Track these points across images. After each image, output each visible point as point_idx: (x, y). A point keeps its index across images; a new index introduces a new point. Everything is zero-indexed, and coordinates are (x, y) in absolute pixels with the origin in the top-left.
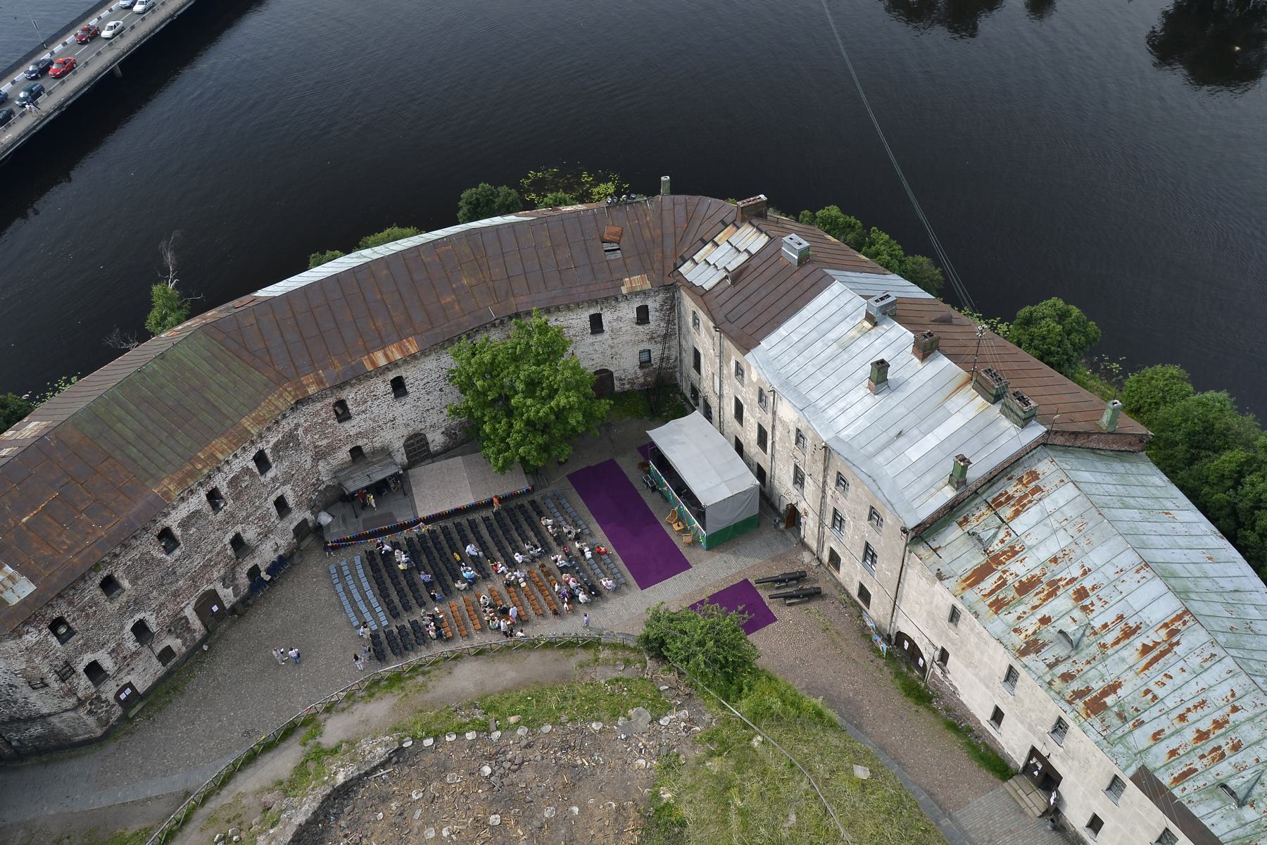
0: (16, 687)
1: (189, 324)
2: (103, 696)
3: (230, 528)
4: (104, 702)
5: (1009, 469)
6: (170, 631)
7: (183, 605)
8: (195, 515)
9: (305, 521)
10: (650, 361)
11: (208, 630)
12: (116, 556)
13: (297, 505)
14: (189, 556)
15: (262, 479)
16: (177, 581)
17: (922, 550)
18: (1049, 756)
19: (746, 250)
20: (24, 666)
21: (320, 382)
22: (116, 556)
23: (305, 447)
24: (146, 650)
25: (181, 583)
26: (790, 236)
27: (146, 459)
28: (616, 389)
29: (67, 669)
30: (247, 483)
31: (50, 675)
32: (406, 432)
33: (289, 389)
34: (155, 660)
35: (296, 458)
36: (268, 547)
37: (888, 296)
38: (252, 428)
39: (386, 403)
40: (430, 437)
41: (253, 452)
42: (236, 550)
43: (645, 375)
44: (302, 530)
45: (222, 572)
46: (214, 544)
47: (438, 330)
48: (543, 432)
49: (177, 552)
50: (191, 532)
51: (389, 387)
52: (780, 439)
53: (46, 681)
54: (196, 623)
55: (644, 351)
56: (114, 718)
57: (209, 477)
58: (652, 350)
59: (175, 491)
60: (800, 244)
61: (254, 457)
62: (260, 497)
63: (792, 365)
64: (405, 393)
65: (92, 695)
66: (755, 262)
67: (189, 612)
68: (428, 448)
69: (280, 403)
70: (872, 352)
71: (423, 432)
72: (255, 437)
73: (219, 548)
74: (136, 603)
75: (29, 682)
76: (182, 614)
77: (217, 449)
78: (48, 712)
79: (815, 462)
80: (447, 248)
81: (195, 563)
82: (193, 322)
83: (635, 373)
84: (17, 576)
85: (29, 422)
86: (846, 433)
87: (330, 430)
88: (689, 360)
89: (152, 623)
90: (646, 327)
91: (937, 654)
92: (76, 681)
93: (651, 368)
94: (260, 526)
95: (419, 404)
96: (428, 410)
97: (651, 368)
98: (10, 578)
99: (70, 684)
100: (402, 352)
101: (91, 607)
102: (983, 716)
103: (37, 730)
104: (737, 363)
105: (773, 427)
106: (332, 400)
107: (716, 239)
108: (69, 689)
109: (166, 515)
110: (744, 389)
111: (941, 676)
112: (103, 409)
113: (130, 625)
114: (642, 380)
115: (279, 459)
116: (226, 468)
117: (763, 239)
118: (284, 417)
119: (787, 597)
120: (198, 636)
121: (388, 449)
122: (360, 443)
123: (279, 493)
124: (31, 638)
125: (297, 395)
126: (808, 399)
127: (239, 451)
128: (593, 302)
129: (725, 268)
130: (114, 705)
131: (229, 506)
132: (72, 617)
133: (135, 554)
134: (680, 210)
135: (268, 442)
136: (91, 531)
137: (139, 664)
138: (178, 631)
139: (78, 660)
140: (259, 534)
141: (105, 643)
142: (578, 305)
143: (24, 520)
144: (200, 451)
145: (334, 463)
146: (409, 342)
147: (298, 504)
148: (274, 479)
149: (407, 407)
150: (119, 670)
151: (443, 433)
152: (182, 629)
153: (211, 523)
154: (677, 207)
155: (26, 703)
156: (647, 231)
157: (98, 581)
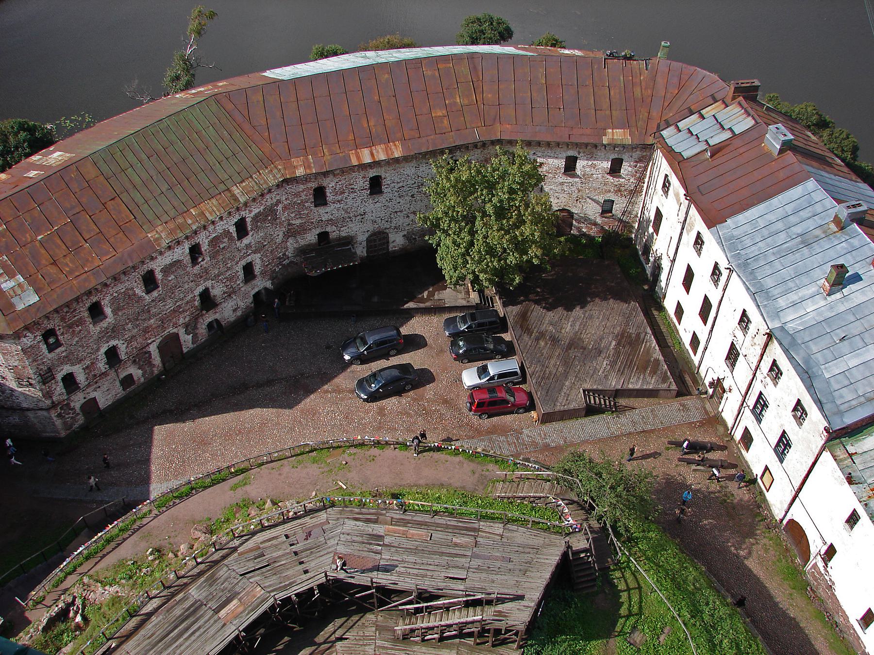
1: (202, 89)
2: (72, 405)
3: (202, 282)
8: (177, 264)
11: (164, 367)
13: (261, 273)
14: (164, 300)
15: (238, 243)
16: (150, 319)
19: (730, 129)
21: (307, 166)
23: (280, 223)
24: (112, 373)
26: (776, 126)
29: (49, 374)
30: (224, 245)
32: (371, 227)
34: (118, 383)
36: (230, 305)
40: (392, 237)
45: (187, 319)
46: (186, 293)
47: (424, 140)
49: (155, 294)
50: (170, 279)
54: (157, 359)
57: (195, 232)
60: (785, 135)
61: (236, 222)
63: (753, 248)
64: (380, 192)
67: (153, 349)
68: (388, 246)
70: (832, 254)
72: (241, 205)
73: (189, 297)
74: (113, 331)
78: (27, 406)
81: (167, 307)
82: (206, 88)
84: (26, 285)
87: (306, 212)
89: (123, 351)
91: (825, 548)
96: (396, 212)
99: (49, 387)
100: (387, 154)
103: (15, 419)
107: (703, 112)
109: (152, 259)
111: (822, 570)
113: (104, 349)
115: (256, 228)
116: (211, 228)
117: (749, 122)
122: (329, 229)
126: (762, 285)
129: (706, 141)
130: (78, 414)
131: (205, 261)
135: (250, 211)
137: (105, 384)
138: (141, 363)
139: (59, 369)
140: (224, 293)
141: (82, 360)
143: (39, 238)
145: (302, 243)
146: (395, 145)
147: (263, 273)
148: (248, 246)
150: (89, 385)
151: (404, 236)
153: (188, 274)
155: (12, 395)
156: (639, 89)
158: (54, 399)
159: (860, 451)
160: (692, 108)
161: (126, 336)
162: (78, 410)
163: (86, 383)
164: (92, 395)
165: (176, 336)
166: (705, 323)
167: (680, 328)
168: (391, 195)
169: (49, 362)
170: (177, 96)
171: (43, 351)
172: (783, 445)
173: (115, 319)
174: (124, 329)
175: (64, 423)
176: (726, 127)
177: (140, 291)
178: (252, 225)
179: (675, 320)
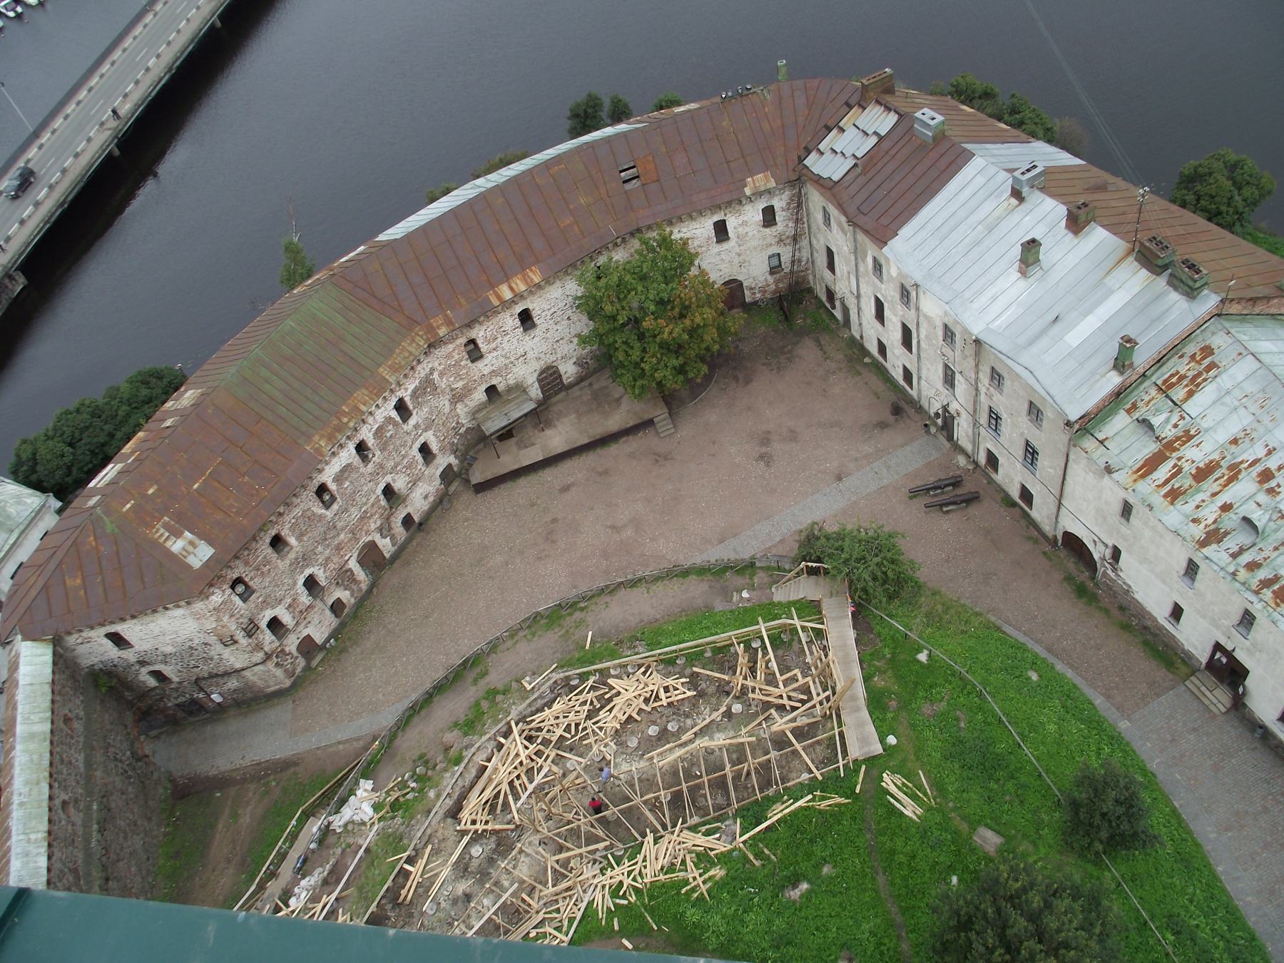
0: (210, 645)
2: (287, 649)
5: (1179, 346)
6: (338, 583)
8: (347, 468)
9: (450, 466)
12: (281, 514)
13: (440, 450)
15: (405, 427)
17: (1089, 443)
18: (1234, 650)
19: (875, 133)
21: (449, 322)
22: (281, 514)
24: (319, 604)
25: (342, 536)
28: (747, 300)
29: (252, 626)
30: (391, 433)
31: (238, 632)
32: (538, 366)
33: (420, 333)
34: (328, 612)
35: (434, 403)
37: (1035, 167)
40: (562, 369)
42: (388, 500)
43: (776, 282)
44: (448, 475)
45: (379, 523)
46: (367, 495)
49: (335, 507)
50: (346, 486)
51: (518, 322)
52: (927, 337)
53: (236, 638)
54: (360, 574)
55: (773, 255)
56: (299, 670)
57: (356, 430)
60: (933, 119)
62: (405, 446)
64: (534, 326)
67: (353, 564)
68: (561, 380)
71: (555, 364)
73: (373, 499)
76: (347, 567)
77: (359, 401)
78: (241, 666)
79: (965, 358)
80: (560, 167)
81: (353, 516)
82: (321, 275)
83: (766, 280)
84: (197, 541)
85: (186, 391)
87: (464, 371)
88: (821, 260)
90: (773, 229)
92: (261, 636)
93: (782, 274)
94: (409, 475)
96: (557, 341)
98: (191, 543)
99: (256, 639)
100: (527, 284)
101: (265, 566)
102: (1161, 613)
103: (233, 683)
104: (875, 259)
106: (463, 340)
107: (841, 124)
111: (1112, 575)
113: (301, 581)
114: (773, 287)
115: (418, 405)
116: (370, 420)
118: (419, 362)
119: (941, 506)
120: (364, 587)
121: (522, 386)
122: (494, 382)
123: (422, 440)
124: (217, 598)
129: (854, 155)
130: (297, 658)
131: (377, 457)
132: (249, 577)
133: (297, 511)
135: (406, 389)
136: (254, 492)
137: (314, 616)
138: (346, 583)
139: (260, 616)
143: (196, 486)
144: (344, 404)
146: (531, 271)
147: (442, 449)
148: (416, 426)
149: (536, 339)
150: (297, 624)
151: (574, 363)
153: (363, 474)
157: (268, 540)
158: (266, 649)
159: (1110, 434)
160: (829, 124)
161: (320, 560)
162: (295, 653)
163: (295, 622)
164: (305, 633)
165: (372, 546)
166: (910, 351)
167: (888, 366)
168: (546, 325)
169: (247, 613)
170: (295, 292)
171: (237, 603)
172: (1031, 454)
173: (302, 546)
174: (315, 554)
175: (285, 671)
176: (870, 132)
177: (319, 510)
178: (412, 403)
179: (881, 359)
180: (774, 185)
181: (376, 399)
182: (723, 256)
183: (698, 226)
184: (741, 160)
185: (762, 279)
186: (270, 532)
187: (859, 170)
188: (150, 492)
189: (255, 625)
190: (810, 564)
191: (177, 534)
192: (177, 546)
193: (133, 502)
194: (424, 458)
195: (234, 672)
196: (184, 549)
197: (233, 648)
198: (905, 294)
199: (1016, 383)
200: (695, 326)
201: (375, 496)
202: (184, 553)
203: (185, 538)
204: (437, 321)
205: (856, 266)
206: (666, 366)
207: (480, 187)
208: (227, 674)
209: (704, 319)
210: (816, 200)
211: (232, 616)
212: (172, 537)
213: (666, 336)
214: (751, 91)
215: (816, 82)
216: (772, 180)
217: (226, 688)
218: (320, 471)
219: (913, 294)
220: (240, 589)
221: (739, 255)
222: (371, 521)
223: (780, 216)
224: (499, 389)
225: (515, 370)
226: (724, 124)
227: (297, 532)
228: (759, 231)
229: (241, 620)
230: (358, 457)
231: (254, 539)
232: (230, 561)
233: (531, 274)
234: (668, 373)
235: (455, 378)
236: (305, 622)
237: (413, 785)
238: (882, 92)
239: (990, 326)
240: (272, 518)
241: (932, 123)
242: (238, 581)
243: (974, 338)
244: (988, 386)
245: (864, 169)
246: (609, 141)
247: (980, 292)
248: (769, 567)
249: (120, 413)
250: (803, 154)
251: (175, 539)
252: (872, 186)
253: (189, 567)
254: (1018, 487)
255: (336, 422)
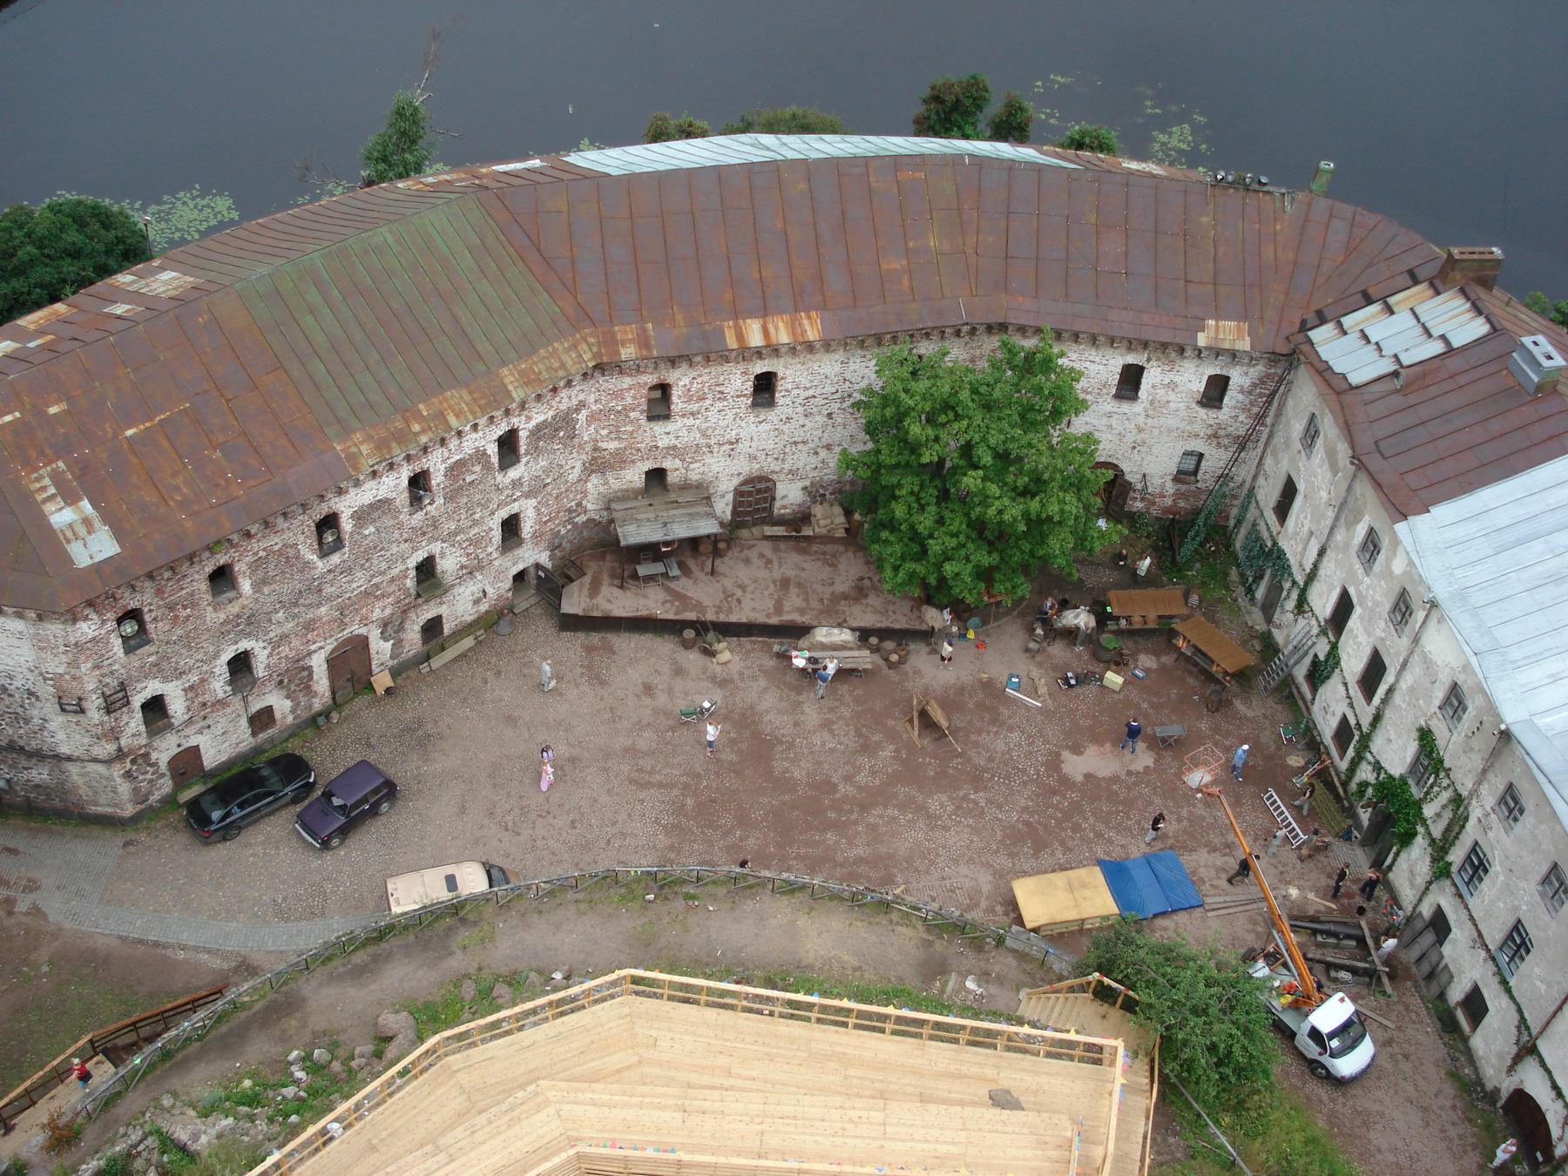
0: (37, 698)
2: (154, 756)
3: (424, 544)
4: (152, 765)
6: (281, 682)
7: (313, 647)
8: (382, 505)
10: (1195, 472)
11: (334, 699)
12: (248, 535)
15: (499, 477)
16: (320, 605)
19: (1443, 337)
20: (61, 670)
21: (643, 342)
22: (248, 535)
23: (580, 445)
24: (236, 701)
25: (323, 610)
27: (336, 390)
29: (120, 695)
30: (474, 477)
31: (94, 697)
33: (591, 340)
34: (244, 722)
36: (468, 592)
38: (515, 388)
39: (734, 411)
40: (781, 489)
41: (501, 429)
42: (419, 582)
43: (1178, 495)
45: (388, 612)
48: (991, 546)
49: (335, 559)
50: (366, 532)
52: (1412, 689)
53: (85, 704)
54: (322, 683)
56: (156, 796)
57: (425, 450)
58: (1207, 456)
59: (368, 461)
60: (1549, 358)
64: (771, 403)
65: (140, 748)
66: (1454, 364)
67: (318, 663)
68: (771, 506)
69: (569, 359)
71: (774, 477)
75: (60, 698)
76: (307, 662)
77: (450, 407)
79: (1468, 749)
80: (917, 175)
81: (355, 585)
83: (1163, 486)
84: (97, 524)
85: (162, 269)
86: (1549, 719)
87: (629, 428)
88: (1268, 494)
89: (261, 662)
90: (1212, 413)
92: (125, 718)
93: (1193, 487)
94: (468, 555)
95: (785, 428)
96: (796, 443)
97: (1193, 487)
98: (86, 522)
99: (116, 719)
100: (794, 333)
101: (185, 607)
103: (40, 774)
104: (1371, 530)
105: (1404, 665)
106: (650, 379)
107: (1392, 300)
108: (112, 729)
110: (1367, 580)
112: (291, 284)
114: (1168, 502)
115: (535, 451)
116: (453, 443)
118: (569, 384)
120: (317, 705)
121: (707, 488)
122: (667, 464)
123: (514, 508)
124: (87, 629)
125: (601, 355)
127: (482, 421)
128: (1131, 345)
129: (1396, 356)
130: (163, 775)
131: (435, 505)
132: (153, 615)
133: (275, 541)
134: (1339, 232)
135: (529, 418)
136: (223, 483)
137: (220, 722)
139: (139, 686)
140: (462, 567)
142: (1112, 341)
143: (129, 432)
144: (424, 401)
146: (809, 318)
147: (537, 536)
148: (516, 484)
149: (764, 427)
150: (190, 722)
151: (805, 488)
152: (298, 685)
153: (400, 526)
154: (1336, 223)
157: (209, 569)
158: (123, 742)
161: (272, 635)
162: (163, 767)
163: (186, 717)
164: (193, 742)
165: (362, 643)
169: (122, 671)
170: (400, 185)
171: (115, 649)
176: (1436, 332)
180: (1248, 348)
181: (479, 414)
182: (1114, 422)
183: (1097, 359)
184: (1210, 288)
185: (1157, 481)
186: (218, 556)
187: (1398, 384)
188: (53, 410)
189: (126, 696)
190: (1106, 981)
191: (71, 499)
192: (61, 517)
193: (17, 414)
194: (504, 539)
195: (51, 757)
196: (70, 526)
197: (74, 718)
198: (1402, 608)
199: (1543, 827)
200: (1044, 516)
201: (402, 567)
202: (69, 534)
203: (79, 508)
204: (626, 333)
205: (1332, 529)
206: (968, 560)
207: (769, 149)
208: (39, 756)
209: (1062, 511)
210: (1304, 397)
211: (97, 667)
212: (59, 499)
213: (992, 512)
214: (1265, 189)
215: (1372, 219)
216: (1248, 339)
217: (25, 775)
218: (341, 492)
219: (1420, 615)
220: (129, 628)
221: (1140, 430)
222: (379, 604)
223: (1232, 398)
224: (669, 479)
225: (708, 459)
226: (1204, 220)
227: (260, 574)
228: (1188, 408)
229: (108, 680)
230: (406, 494)
231: (191, 558)
232: (137, 579)
233: (805, 322)
234: (967, 570)
235: (611, 433)
236: (202, 724)
237: (300, 1075)
238: (1473, 279)
239: (1537, 720)
240: (235, 538)
241: (1546, 363)
242: (134, 615)
243: (1503, 727)
244: (1489, 809)
245: (1408, 384)
246: (1010, 169)
247: (1535, 659)
248: (1027, 954)
249: (19, 253)
250: (1311, 318)
251: (62, 504)
252: (1410, 418)
253: (67, 559)
254: (1468, 986)
255: (399, 424)
